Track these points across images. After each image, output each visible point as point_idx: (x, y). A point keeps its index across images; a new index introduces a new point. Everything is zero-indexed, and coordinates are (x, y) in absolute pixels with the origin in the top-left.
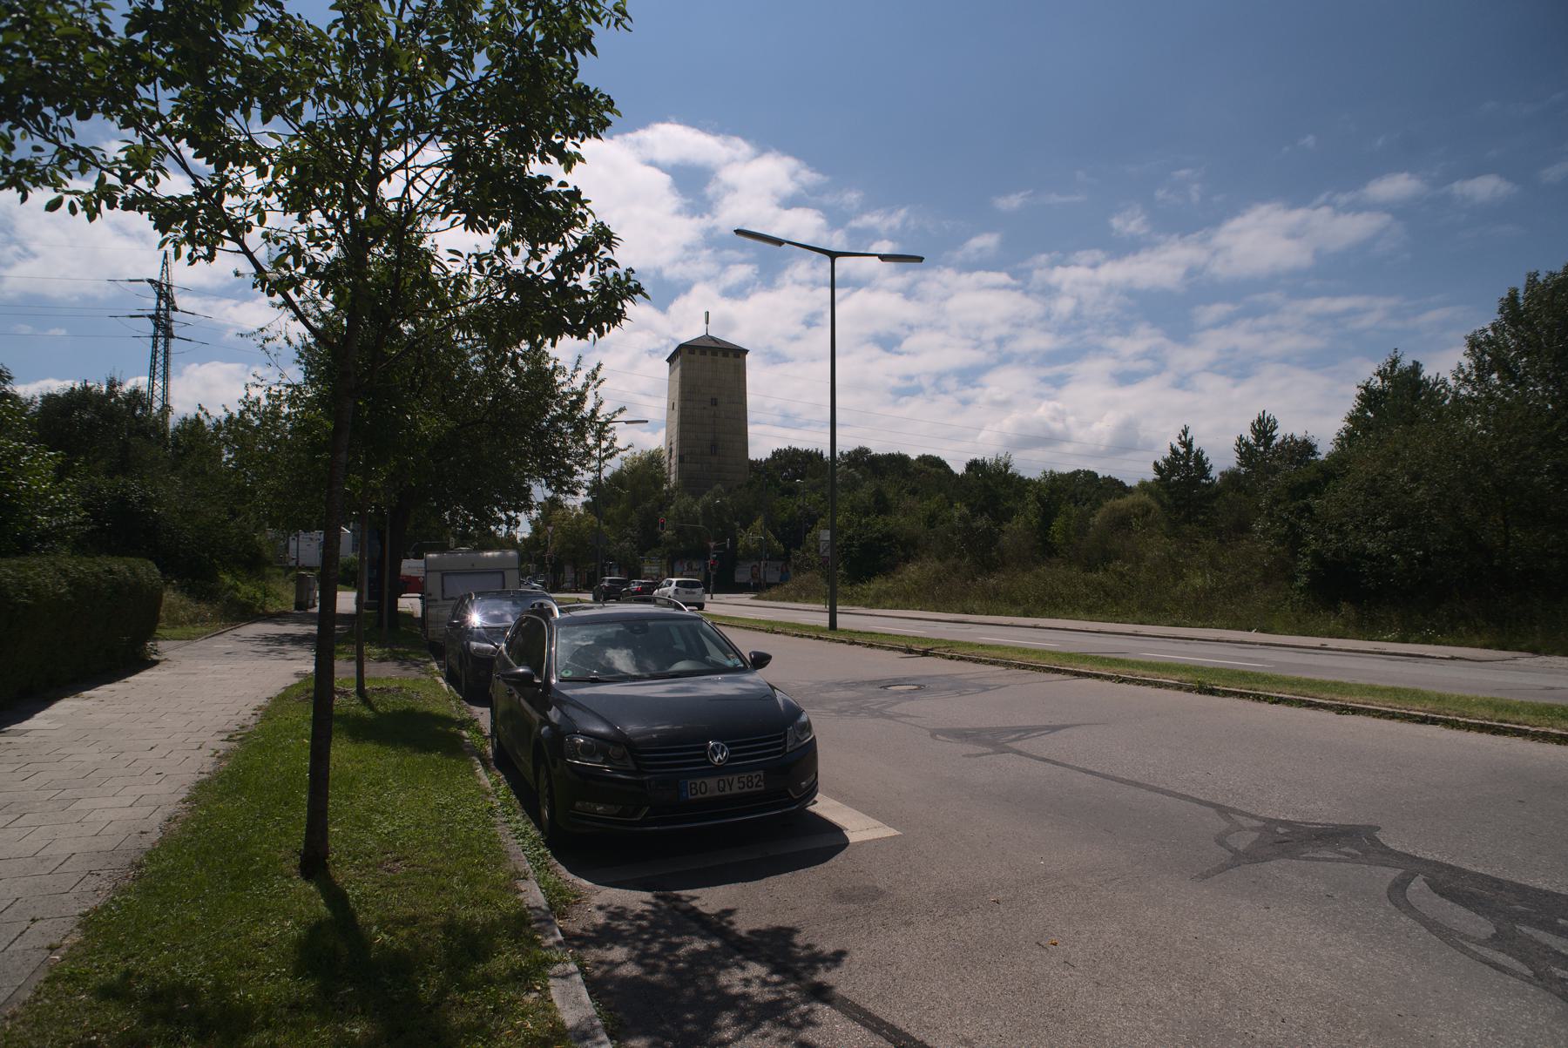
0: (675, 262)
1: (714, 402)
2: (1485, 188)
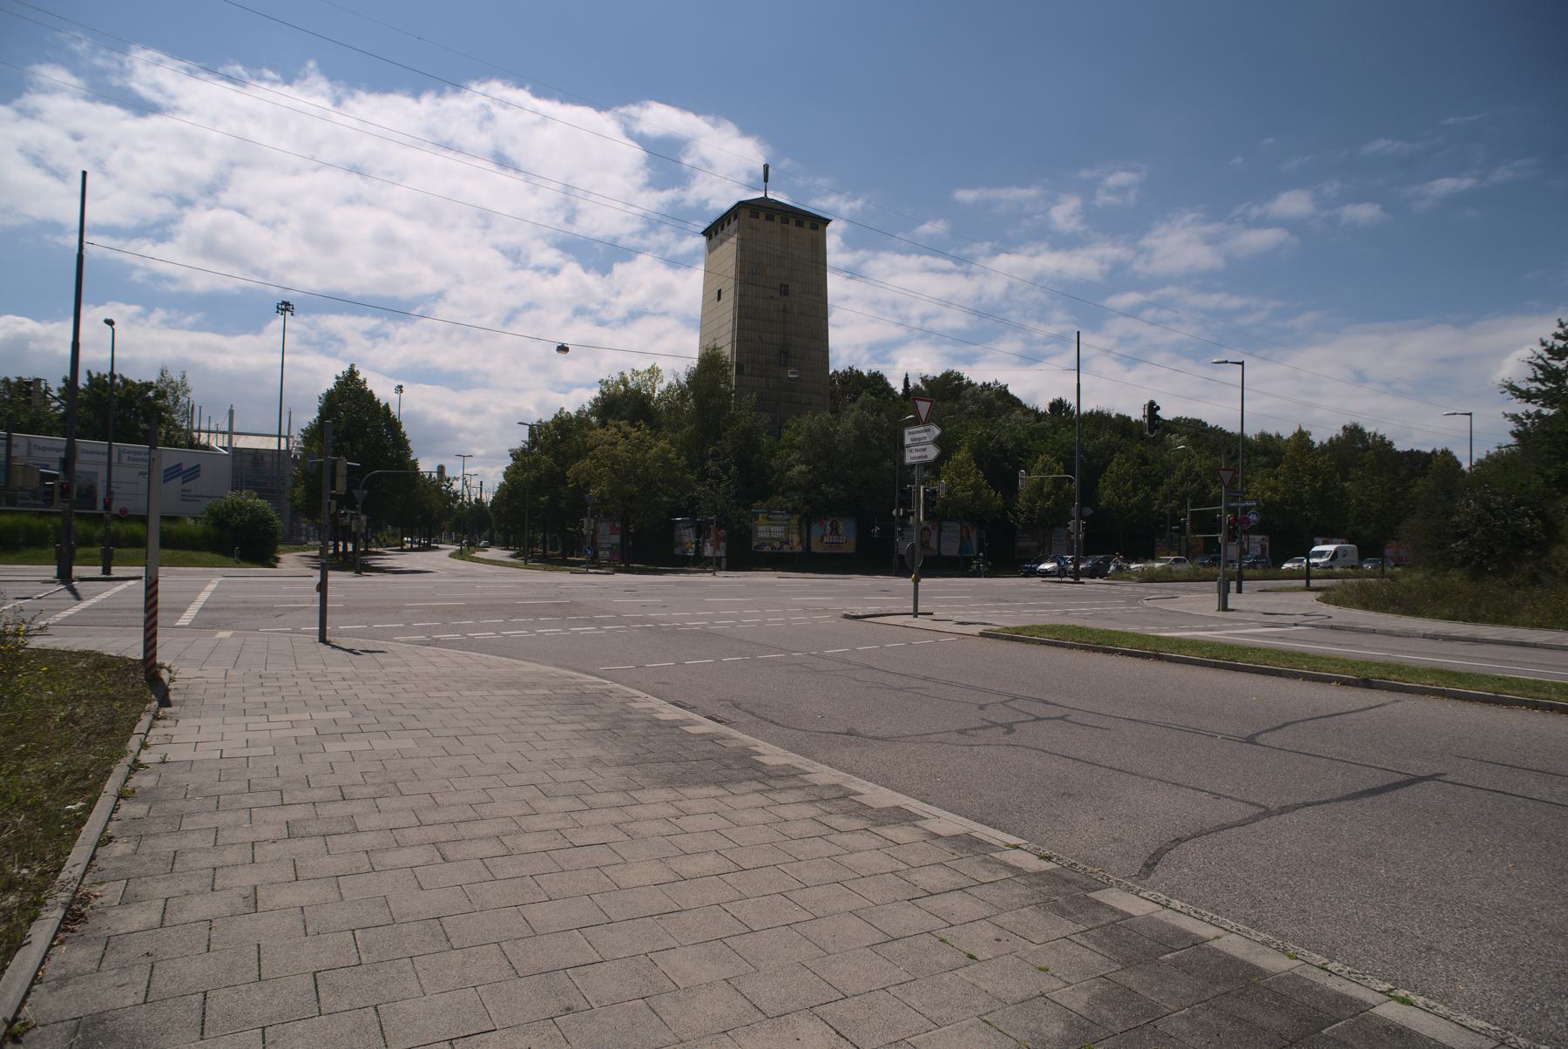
0: (631, 235)
1: (785, 291)
2: (1364, 213)
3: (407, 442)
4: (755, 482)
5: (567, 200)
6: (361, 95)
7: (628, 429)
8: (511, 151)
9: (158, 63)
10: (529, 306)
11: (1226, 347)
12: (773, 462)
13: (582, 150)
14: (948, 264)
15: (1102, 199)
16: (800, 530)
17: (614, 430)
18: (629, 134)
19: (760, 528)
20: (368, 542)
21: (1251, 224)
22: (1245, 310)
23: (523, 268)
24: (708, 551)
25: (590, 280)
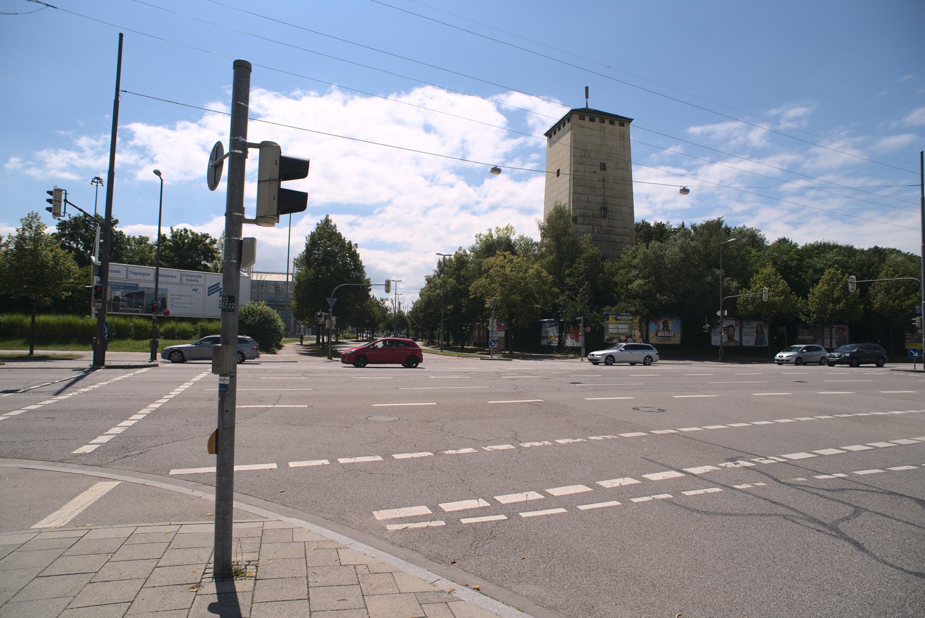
3: (363, 267)
4: (604, 295)
5: (462, 148)
6: (357, 98)
7: (512, 257)
8: (433, 122)
9: (263, 94)
10: (436, 206)
11: (844, 217)
12: (616, 279)
13: (473, 121)
14: (683, 171)
15: (784, 126)
16: (640, 327)
17: (502, 258)
18: (500, 110)
19: (610, 326)
20: (337, 336)
21: (888, 133)
22: (879, 187)
23: (436, 184)
24: (569, 342)
25: (471, 190)
